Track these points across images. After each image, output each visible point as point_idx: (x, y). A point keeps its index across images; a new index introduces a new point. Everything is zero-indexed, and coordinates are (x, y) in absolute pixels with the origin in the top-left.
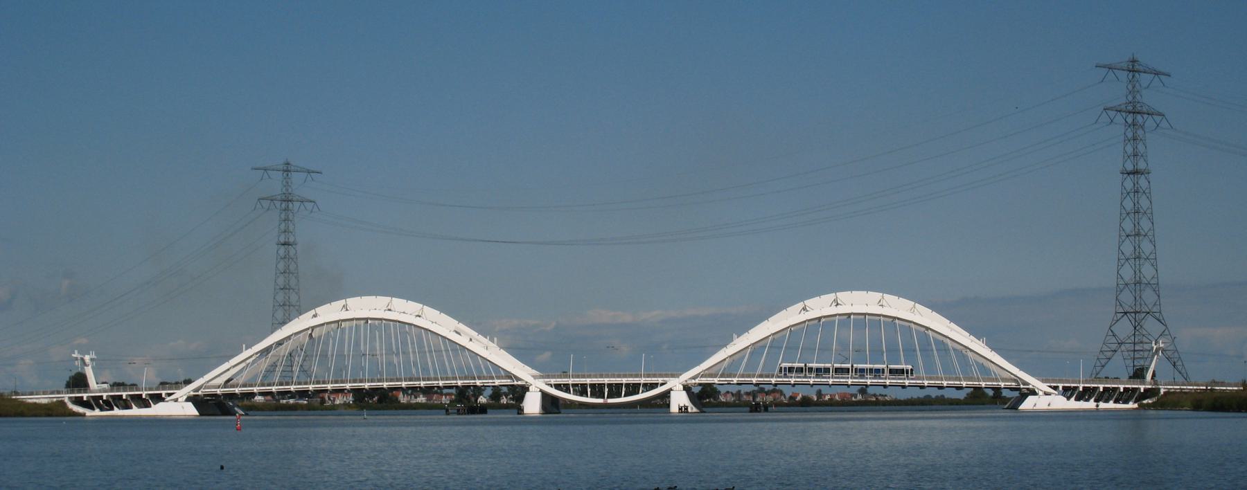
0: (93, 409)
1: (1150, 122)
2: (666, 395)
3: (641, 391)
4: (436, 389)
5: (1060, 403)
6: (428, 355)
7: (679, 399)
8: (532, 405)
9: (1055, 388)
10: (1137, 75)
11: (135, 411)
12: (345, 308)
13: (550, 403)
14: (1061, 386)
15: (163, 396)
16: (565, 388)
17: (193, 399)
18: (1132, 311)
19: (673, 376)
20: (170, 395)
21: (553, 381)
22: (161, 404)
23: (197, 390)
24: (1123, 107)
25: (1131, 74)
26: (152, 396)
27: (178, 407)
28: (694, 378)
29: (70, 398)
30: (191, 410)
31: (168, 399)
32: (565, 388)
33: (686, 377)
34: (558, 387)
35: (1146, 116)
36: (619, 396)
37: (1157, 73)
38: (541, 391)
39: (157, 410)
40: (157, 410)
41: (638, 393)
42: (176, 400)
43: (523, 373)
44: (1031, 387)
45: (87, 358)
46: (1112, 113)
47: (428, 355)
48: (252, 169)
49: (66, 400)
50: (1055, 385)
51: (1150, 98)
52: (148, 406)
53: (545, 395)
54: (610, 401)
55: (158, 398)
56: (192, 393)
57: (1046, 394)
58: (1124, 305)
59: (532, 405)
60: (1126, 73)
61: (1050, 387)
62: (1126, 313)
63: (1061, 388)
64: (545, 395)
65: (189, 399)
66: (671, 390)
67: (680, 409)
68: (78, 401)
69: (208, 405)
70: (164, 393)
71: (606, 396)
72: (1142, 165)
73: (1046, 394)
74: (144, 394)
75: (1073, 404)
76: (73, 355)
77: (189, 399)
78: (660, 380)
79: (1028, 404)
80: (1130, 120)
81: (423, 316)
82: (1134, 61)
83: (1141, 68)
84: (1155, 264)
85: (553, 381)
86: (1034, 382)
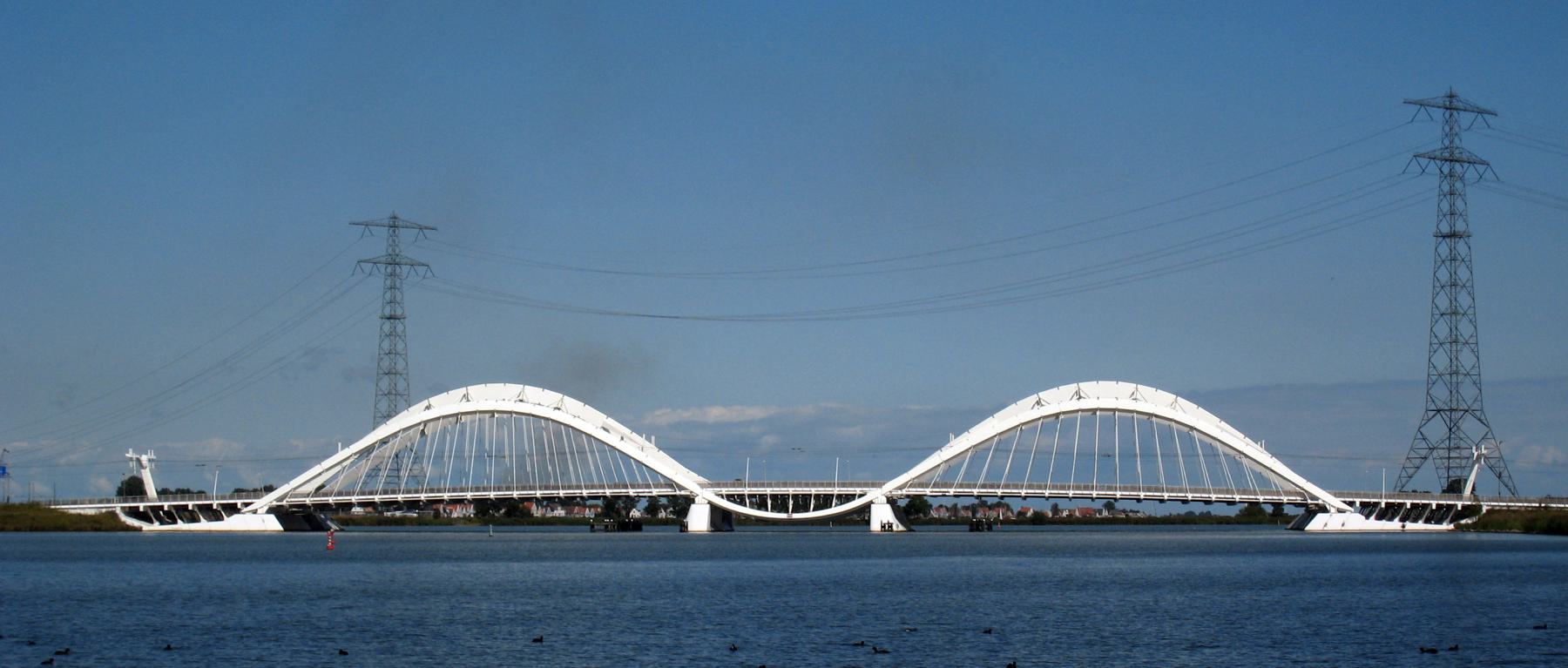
0: (152, 522)
1: (1471, 173)
2: (866, 508)
3: (834, 504)
4: (578, 499)
5: (1357, 522)
6: (569, 456)
7: (882, 515)
8: (698, 520)
9: (1351, 504)
10: (1455, 113)
11: (204, 525)
12: (466, 397)
13: (720, 518)
14: (1358, 501)
15: (239, 506)
16: (740, 499)
17: (276, 511)
18: (1446, 408)
19: (874, 485)
20: (247, 505)
21: (724, 491)
22: (236, 516)
23: (281, 499)
24: (1438, 154)
25: (1448, 113)
26: (224, 507)
27: (257, 520)
28: (900, 488)
29: (122, 508)
30: (273, 524)
31: (245, 510)
32: (740, 499)
33: (891, 486)
34: (730, 498)
35: (1466, 165)
36: (807, 510)
37: (1481, 112)
38: (709, 503)
39: (231, 524)
40: (231, 524)
41: (831, 507)
42: (255, 512)
43: (687, 480)
44: (1320, 502)
45: (144, 458)
46: (1424, 162)
47: (569, 456)
48: (1405, 103)
49: (118, 511)
50: (1351, 500)
51: (1471, 143)
52: (220, 518)
53: (715, 509)
54: (796, 516)
55: (232, 509)
56: (275, 503)
57: (1340, 511)
58: (1435, 399)
59: (698, 520)
60: (1442, 110)
61: (1345, 502)
62: (1439, 411)
63: (1358, 504)
64: (715, 509)
65: (271, 511)
66: (872, 502)
67: (883, 527)
68: (134, 513)
69: (289, 515)
70: (239, 502)
71: (790, 510)
72: (1460, 226)
73: (1340, 511)
74: (215, 504)
75: (1373, 524)
76: (127, 455)
77: (271, 511)
78: (858, 491)
79: (1317, 524)
80: (1446, 169)
81: (563, 408)
82: (1451, 96)
83: (1460, 105)
84: (1476, 349)
85: (724, 491)
86: (1324, 496)
